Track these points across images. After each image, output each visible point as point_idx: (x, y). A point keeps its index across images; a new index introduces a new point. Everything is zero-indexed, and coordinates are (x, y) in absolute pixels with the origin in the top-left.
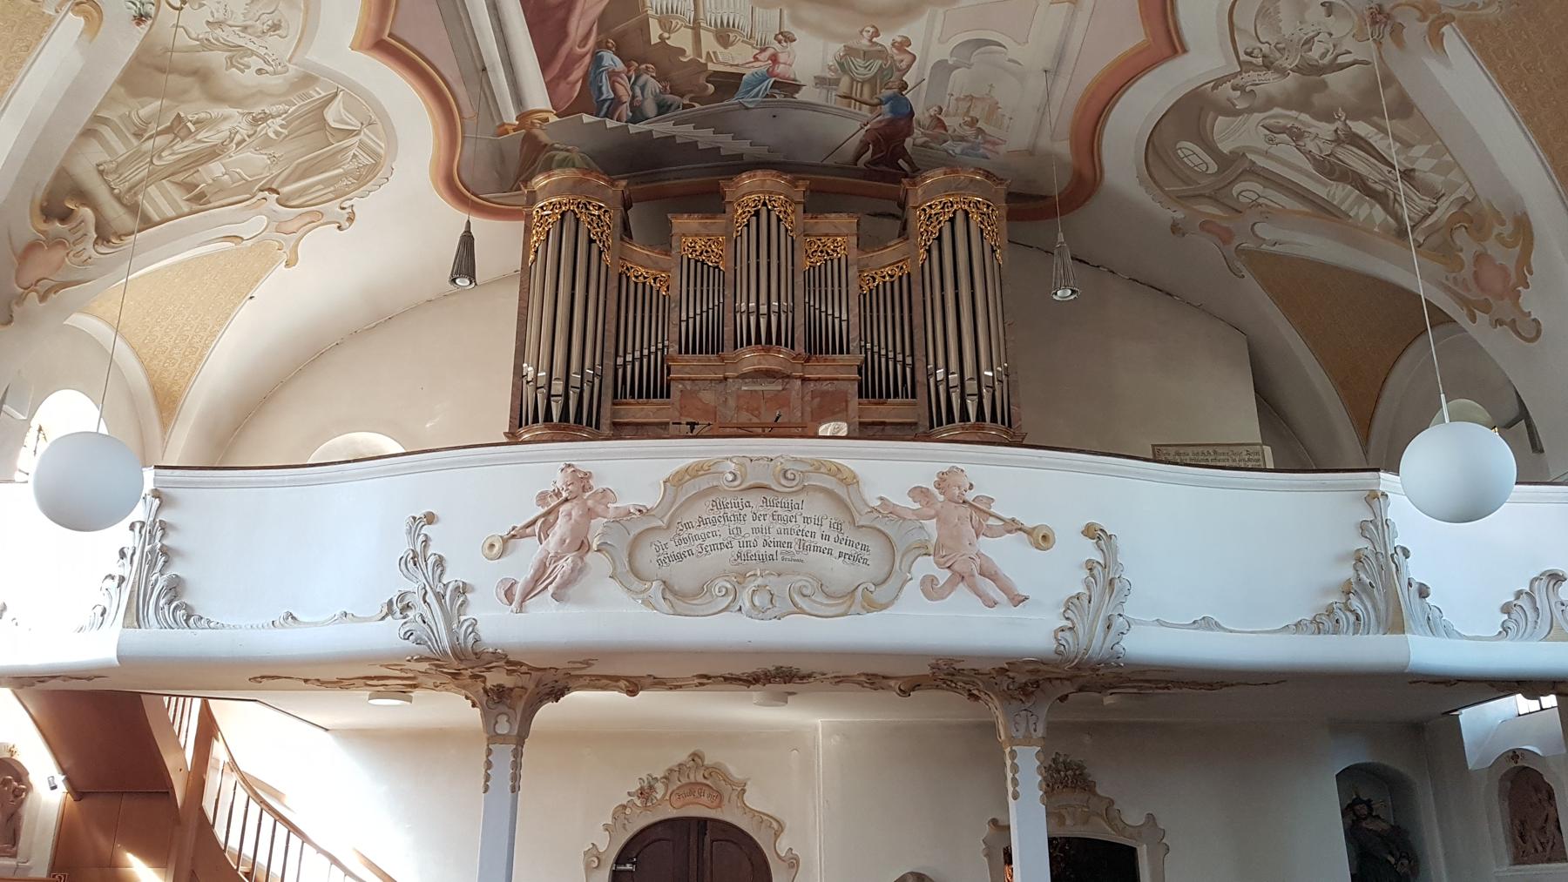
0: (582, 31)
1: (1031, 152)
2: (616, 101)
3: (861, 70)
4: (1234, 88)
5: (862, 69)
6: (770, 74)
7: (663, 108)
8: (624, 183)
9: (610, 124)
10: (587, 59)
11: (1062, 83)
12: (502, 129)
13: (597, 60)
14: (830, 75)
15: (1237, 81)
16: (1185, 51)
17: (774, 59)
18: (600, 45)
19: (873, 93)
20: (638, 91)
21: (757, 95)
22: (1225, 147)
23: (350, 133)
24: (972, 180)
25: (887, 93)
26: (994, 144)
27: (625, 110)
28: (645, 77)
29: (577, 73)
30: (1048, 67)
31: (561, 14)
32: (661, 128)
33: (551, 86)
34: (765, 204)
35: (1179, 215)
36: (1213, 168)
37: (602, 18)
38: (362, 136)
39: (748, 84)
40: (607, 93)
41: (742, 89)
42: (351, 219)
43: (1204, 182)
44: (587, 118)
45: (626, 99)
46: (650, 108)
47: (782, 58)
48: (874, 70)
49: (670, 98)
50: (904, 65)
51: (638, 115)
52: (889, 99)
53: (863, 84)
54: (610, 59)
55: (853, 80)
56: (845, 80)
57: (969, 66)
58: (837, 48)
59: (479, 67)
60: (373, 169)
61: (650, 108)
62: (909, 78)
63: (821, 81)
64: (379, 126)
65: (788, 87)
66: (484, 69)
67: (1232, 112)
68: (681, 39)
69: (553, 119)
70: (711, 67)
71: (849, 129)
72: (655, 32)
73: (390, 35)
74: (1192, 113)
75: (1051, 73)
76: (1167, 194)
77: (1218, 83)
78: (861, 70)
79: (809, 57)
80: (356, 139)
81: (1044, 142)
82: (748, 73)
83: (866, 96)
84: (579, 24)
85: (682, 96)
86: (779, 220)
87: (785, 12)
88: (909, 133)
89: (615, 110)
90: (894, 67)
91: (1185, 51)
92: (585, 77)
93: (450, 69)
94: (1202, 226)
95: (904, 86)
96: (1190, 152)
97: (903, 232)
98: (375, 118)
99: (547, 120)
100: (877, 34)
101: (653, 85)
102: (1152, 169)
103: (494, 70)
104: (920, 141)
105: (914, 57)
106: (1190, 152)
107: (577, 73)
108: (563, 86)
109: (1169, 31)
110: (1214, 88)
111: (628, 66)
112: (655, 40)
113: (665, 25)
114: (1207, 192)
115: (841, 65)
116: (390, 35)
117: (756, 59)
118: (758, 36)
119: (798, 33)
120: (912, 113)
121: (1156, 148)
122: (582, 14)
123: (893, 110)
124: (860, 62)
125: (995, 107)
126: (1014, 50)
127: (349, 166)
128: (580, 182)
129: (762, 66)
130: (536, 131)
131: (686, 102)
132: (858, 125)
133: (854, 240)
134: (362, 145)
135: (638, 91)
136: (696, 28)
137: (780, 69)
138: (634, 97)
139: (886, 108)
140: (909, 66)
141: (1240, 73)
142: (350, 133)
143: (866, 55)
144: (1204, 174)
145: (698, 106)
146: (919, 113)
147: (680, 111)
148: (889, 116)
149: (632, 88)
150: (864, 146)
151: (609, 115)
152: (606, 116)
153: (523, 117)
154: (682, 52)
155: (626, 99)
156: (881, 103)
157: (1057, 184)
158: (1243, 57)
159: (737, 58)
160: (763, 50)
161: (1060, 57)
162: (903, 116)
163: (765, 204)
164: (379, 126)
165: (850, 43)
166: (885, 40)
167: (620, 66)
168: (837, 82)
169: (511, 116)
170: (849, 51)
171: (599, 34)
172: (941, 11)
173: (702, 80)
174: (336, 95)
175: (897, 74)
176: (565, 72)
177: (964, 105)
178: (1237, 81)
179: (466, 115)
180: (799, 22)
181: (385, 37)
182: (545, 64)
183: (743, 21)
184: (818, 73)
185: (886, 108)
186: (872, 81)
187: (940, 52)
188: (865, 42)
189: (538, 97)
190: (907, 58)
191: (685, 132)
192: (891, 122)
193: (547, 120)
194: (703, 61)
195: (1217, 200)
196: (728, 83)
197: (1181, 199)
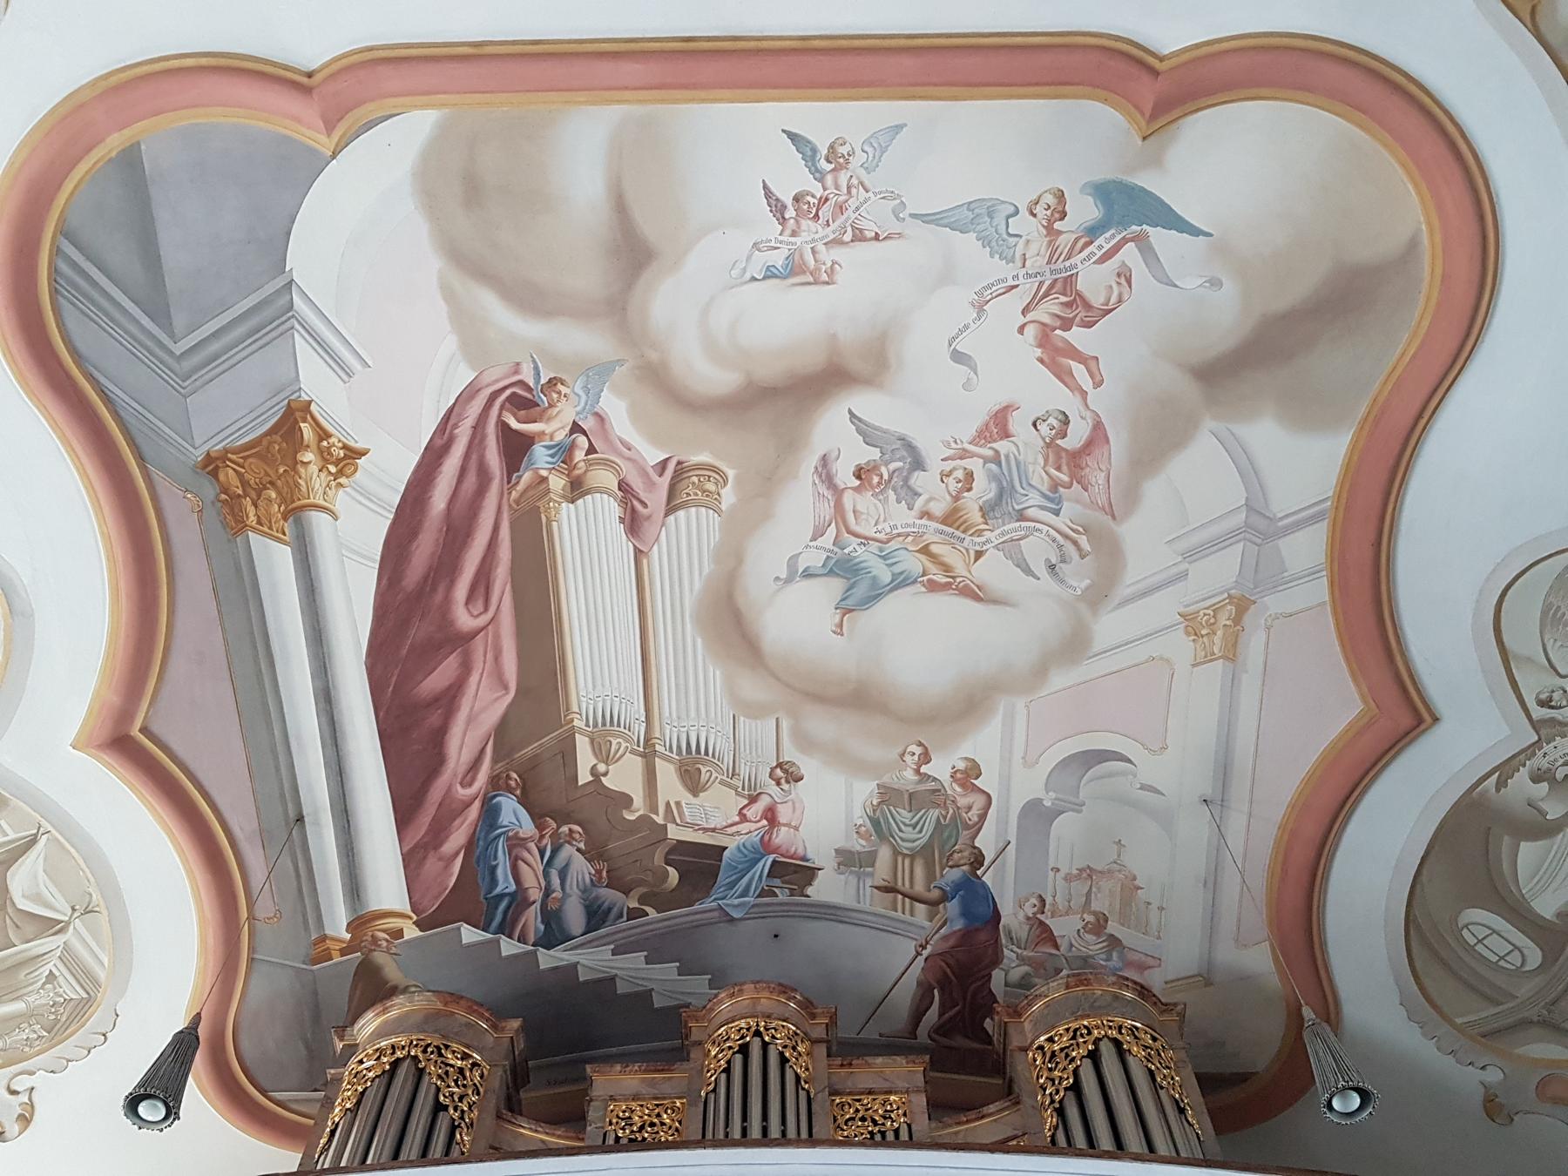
0: (467, 756)
1: (1205, 978)
2: (519, 900)
3: (909, 833)
4: (1536, 779)
5: (914, 830)
6: (766, 846)
7: (596, 916)
8: (515, 1024)
9: (509, 947)
10: (474, 811)
11: (1236, 825)
12: (320, 950)
13: (490, 813)
14: (859, 845)
15: (1539, 761)
16: (1436, 720)
17: (771, 815)
18: (497, 784)
19: (930, 876)
20: (556, 881)
21: (744, 894)
22: (1546, 906)
23: (50, 926)
24: (1116, 997)
25: (953, 875)
26: (1142, 967)
27: (532, 918)
28: (567, 851)
29: (457, 839)
30: (1208, 792)
31: (434, 719)
32: (591, 959)
33: (412, 861)
34: (758, 1033)
35: (1493, 1076)
36: (1535, 957)
37: (502, 730)
38: (69, 935)
39: (731, 867)
40: (505, 883)
41: (722, 878)
42: (25, 1120)
43: (1525, 990)
44: (469, 934)
45: (535, 895)
46: (575, 917)
47: (784, 814)
48: (929, 829)
49: (609, 895)
50: (973, 816)
51: (553, 935)
52: (959, 886)
53: (912, 857)
54: (512, 813)
55: (896, 853)
56: (884, 853)
57: (1078, 807)
58: (865, 791)
59: (292, 814)
60: (82, 1008)
61: (575, 917)
62: (986, 842)
63: (848, 860)
64: (103, 919)
65: (795, 873)
66: (300, 819)
67: (1543, 830)
68: (624, 777)
69: (411, 932)
70: (675, 833)
71: (894, 958)
72: (585, 760)
73: (144, 730)
74: (1471, 843)
75: (1215, 803)
76: (1459, 1029)
77: (1505, 771)
78: (909, 833)
79: (826, 813)
80: (59, 940)
81: (1228, 955)
82: (732, 844)
83: (919, 887)
84: (466, 738)
85: (626, 893)
86: (784, 1061)
87: (785, 724)
88: (996, 960)
89: (515, 921)
90: (957, 823)
91: (1436, 720)
92: (470, 846)
93: (243, 822)
94: (1542, 1085)
95: (978, 860)
96: (1487, 931)
97: (1009, 1092)
98: (98, 902)
99: (399, 933)
100: (926, 758)
101: (581, 868)
102: (1427, 982)
103: (317, 823)
104: (1017, 973)
105: (989, 797)
106: (1487, 931)
107: (457, 839)
108: (431, 865)
109: (1357, 785)
110: (1501, 784)
111: (540, 827)
112: (584, 777)
113: (603, 752)
114: (1532, 1013)
115: (876, 823)
116: (144, 730)
117: (743, 818)
118: (744, 771)
119: (807, 765)
120: (997, 916)
121: (1424, 934)
122: (470, 720)
123: (965, 913)
124: (904, 815)
125: (1130, 887)
126: (1148, 768)
127: (38, 998)
128: (437, 1014)
129: (751, 832)
130: (380, 958)
131: (634, 904)
132: (910, 947)
133: (921, 1100)
134: (68, 957)
135: (556, 881)
136: (648, 754)
137: (781, 837)
138: (548, 892)
139: (953, 907)
140: (983, 817)
141: (1537, 744)
142: (50, 926)
143: (914, 801)
144: (1519, 973)
145: (652, 913)
146: (1012, 916)
147: (623, 924)
148: (959, 925)
149: (546, 874)
150: (925, 990)
151: (506, 928)
152: (501, 930)
153: (360, 923)
154: (627, 801)
155: (535, 895)
156: (945, 898)
157: (1259, 1046)
158: (1538, 713)
159: (709, 815)
160: (753, 800)
161: (1224, 770)
162: (982, 917)
163: (758, 1033)
164: (103, 919)
165: (886, 779)
166: (941, 768)
167: (527, 827)
168: (869, 859)
169: (338, 923)
170: (888, 795)
171: (495, 761)
172: (1020, 704)
173: (658, 858)
174: (33, 841)
175: (965, 835)
176: (439, 832)
177: (1080, 888)
178: (1539, 761)
179: (260, 913)
180: (806, 743)
181: (135, 732)
182: (404, 814)
183: (720, 744)
184: (841, 844)
185: (953, 907)
186: (926, 852)
187: (1029, 784)
188: (909, 775)
189: (388, 889)
190: (979, 801)
191: (632, 969)
192: (966, 936)
193: (399, 933)
194: (659, 820)
195: (1556, 1028)
196: (701, 865)
197: (1492, 1036)
